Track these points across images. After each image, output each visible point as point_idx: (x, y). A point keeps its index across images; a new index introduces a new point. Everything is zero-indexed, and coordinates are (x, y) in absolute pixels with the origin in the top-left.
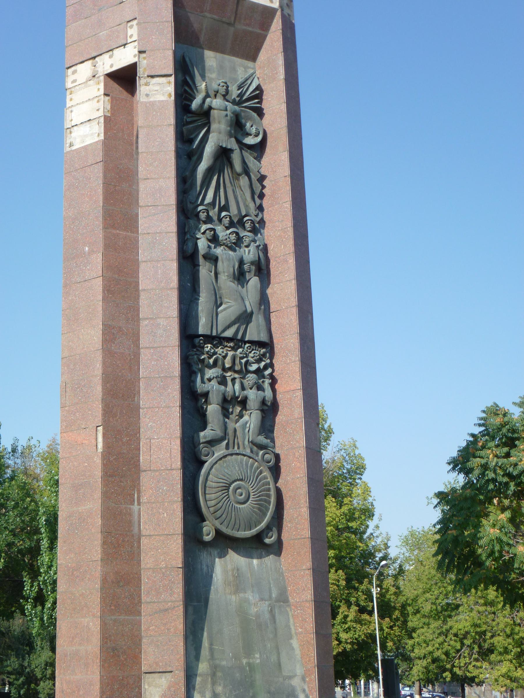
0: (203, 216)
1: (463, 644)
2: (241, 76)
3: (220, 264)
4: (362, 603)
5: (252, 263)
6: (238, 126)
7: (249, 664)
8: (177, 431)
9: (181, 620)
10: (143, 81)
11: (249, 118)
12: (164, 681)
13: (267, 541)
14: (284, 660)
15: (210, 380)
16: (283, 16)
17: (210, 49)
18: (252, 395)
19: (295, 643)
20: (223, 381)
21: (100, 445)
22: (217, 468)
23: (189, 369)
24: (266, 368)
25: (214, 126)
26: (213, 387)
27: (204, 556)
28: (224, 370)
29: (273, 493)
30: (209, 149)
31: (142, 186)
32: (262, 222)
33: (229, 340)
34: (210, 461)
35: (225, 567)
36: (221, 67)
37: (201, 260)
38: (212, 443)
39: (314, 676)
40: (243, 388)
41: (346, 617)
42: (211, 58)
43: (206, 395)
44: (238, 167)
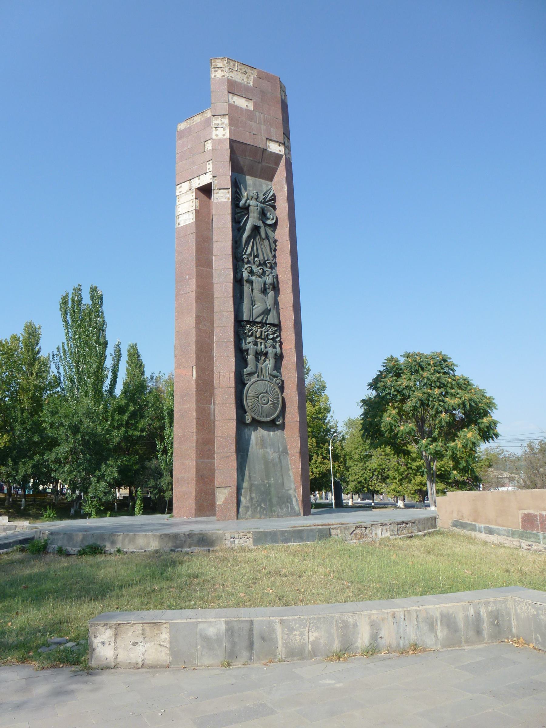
0: (245, 260)
1: (373, 474)
3: (254, 284)
4: (324, 455)
5: (270, 284)
6: (263, 214)
7: (268, 483)
10: (215, 191)
11: (269, 211)
12: (226, 491)
13: (277, 423)
15: (249, 343)
16: (286, 159)
17: (249, 175)
18: (270, 350)
19: (291, 473)
20: (255, 344)
21: (194, 376)
22: (253, 387)
23: (239, 337)
24: (277, 337)
26: (251, 347)
27: (246, 430)
28: (256, 338)
29: (280, 399)
30: (249, 226)
32: (275, 264)
33: (258, 323)
35: (257, 436)
36: (255, 184)
37: (245, 283)
38: (250, 374)
40: (266, 347)
41: (316, 461)
42: (249, 180)
43: (247, 350)
44: (263, 236)
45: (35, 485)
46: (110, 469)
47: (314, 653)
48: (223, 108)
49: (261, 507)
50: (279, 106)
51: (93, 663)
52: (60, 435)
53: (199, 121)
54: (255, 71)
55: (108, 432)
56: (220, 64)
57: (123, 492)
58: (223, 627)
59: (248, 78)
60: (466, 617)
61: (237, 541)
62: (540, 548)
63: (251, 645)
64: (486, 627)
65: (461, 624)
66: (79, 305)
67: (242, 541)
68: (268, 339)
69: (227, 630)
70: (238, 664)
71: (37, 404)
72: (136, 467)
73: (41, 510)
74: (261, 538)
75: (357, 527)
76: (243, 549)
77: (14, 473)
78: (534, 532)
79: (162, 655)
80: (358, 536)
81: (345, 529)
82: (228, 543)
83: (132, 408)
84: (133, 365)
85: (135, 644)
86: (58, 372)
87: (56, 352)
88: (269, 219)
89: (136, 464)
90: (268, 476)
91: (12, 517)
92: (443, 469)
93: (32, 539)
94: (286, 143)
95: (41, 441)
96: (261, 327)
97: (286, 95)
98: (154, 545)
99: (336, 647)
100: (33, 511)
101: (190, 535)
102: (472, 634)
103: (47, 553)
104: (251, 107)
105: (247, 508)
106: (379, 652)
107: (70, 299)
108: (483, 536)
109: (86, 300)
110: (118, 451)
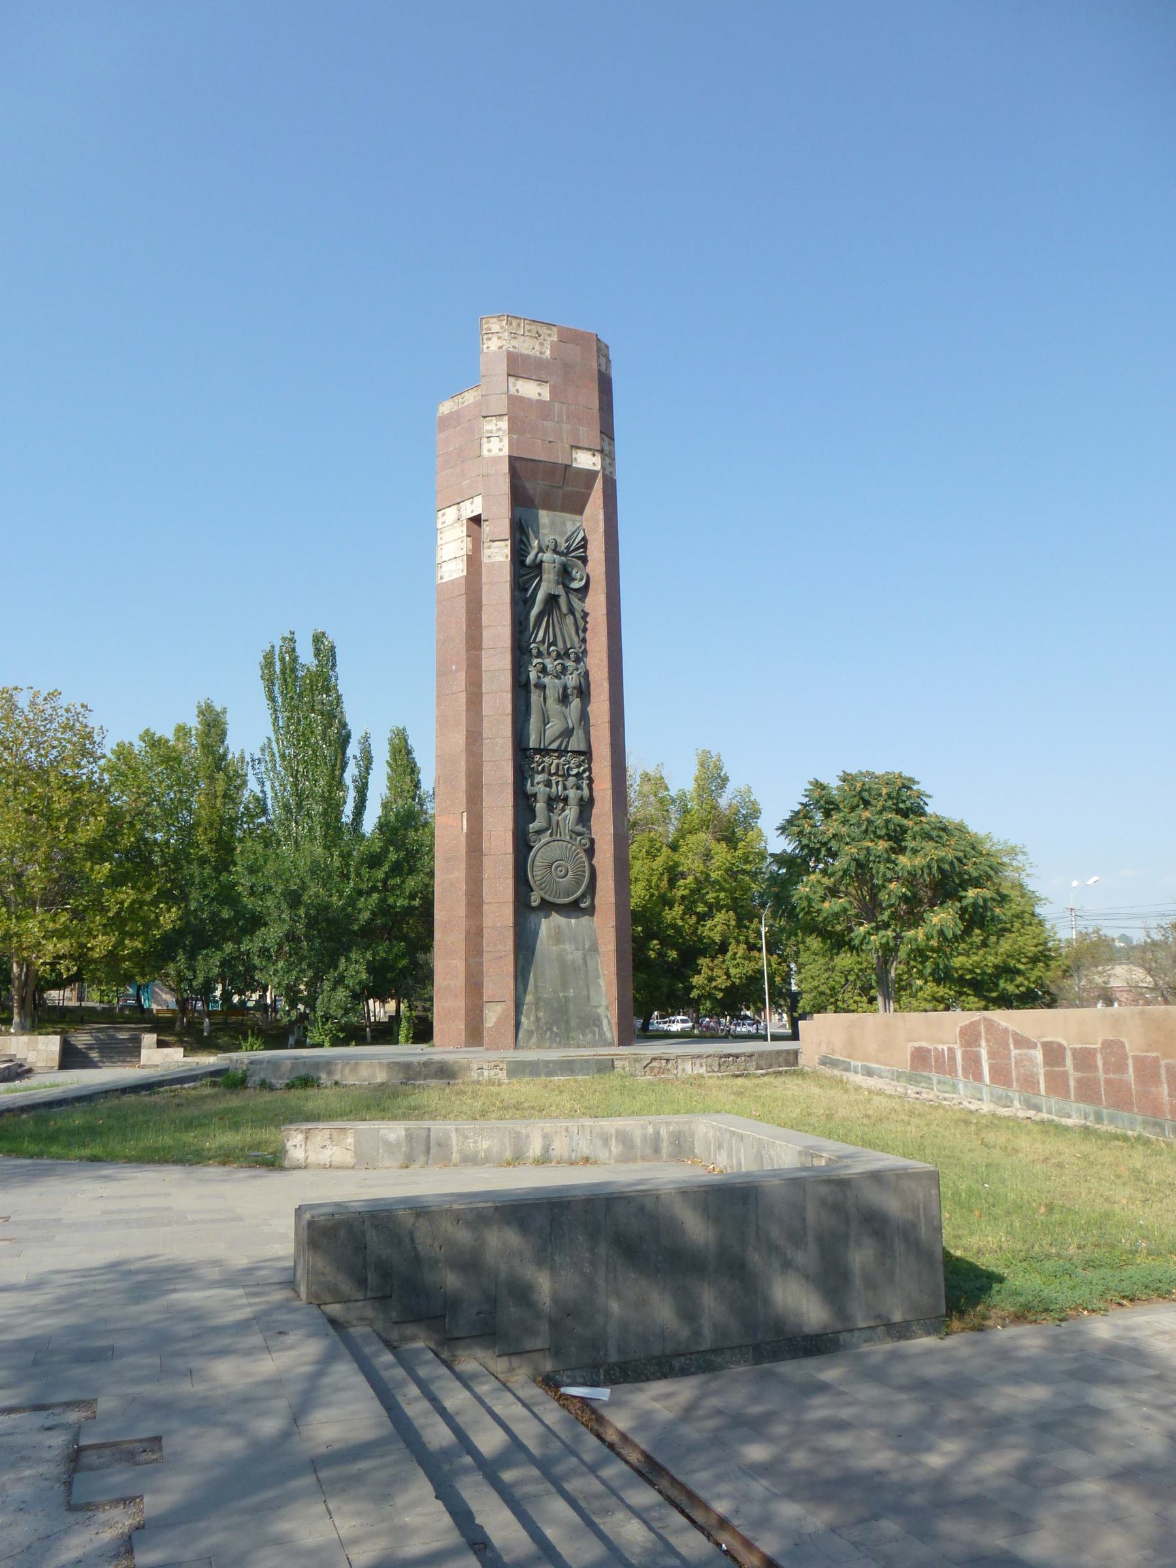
0: (534, 652)
1: (847, 980)
2: (570, 528)
3: (547, 691)
4: (752, 941)
5: (574, 688)
6: (565, 574)
7: (565, 997)
8: (510, 825)
9: (512, 964)
10: (486, 545)
11: (575, 566)
12: (499, 1008)
13: (582, 905)
14: (592, 994)
16: (604, 476)
17: (544, 508)
18: (572, 793)
19: (602, 982)
20: (548, 784)
21: (465, 827)
22: (543, 853)
23: (521, 774)
24: (584, 771)
25: (545, 576)
26: (541, 790)
27: (533, 918)
28: (550, 774)
29: (587, 869)
30: (540, 596)
31: (485, 632)
32: (585, 652)
33: (554, 751)
34: (537, 846)
35: (548, 926)
36: (553, 524)
37: (533, 688)
38: (539, 832)
39: (615, 1007)
40: (565, 788)
41: (735, 954)
42: (544, 516)
43: (535, 795)
44: (564, 609)
45: (226, 996)
46: (355, 968)
47: (486, 1160)
48: (502, 405)
49: (552, 1032)
50: (595, 386)
51: (286, 1164)
52: (268, 908)
53: (472, 401)
54: (555, 329)
55: (351, 901)
56: (495, 327)
57: (380, 1010)
58: (403, 1133)
59: (541, 344)
60: (644, 1136)
61: (486, 1073)
62: (931, 1096)
63: (428, 1151)
64: (665, 1147)
65: (638, 1141)
66: (293, 670)
67: (492, 1073)
68: (569, 775)
69: (406, 1136)
70: (415, 1168)
71: (224, 846)
72: (403, 963)
73: (237, 1039)
74: (517, 1069)
75: (654, 1059)
76: (491, 1082)
77: (189, 975)
78: (926, 1074)
79: (349, 1158)
80: (656, 1071)
81: (636, 1061)
82: (474, 1075)
83: (393, 856)
84: (400, 770)
85: (324, 1147)
86: (263, 792)
87: (258, 755)
88: (574, 579)
89: (404, 956)
90: (565, 986)
91: (190, 1050)
92: (978, 971)
93: (227, 1070)
94: (607, 448)
95: (234, 917)
96: (559, 758)
97: (608, 361)
98: (381, 1077)
99: (508, 1155)
100: (224, 1040)
101: (426, 1064)
102: (648, 1151)
103: (246, 1088)
104: (546, 396)
105: (530, 1033)
106: (550, 1162)
107: (276, 656)
108: (859, 1079)
109: (306, 656)
110: (369, 934)
